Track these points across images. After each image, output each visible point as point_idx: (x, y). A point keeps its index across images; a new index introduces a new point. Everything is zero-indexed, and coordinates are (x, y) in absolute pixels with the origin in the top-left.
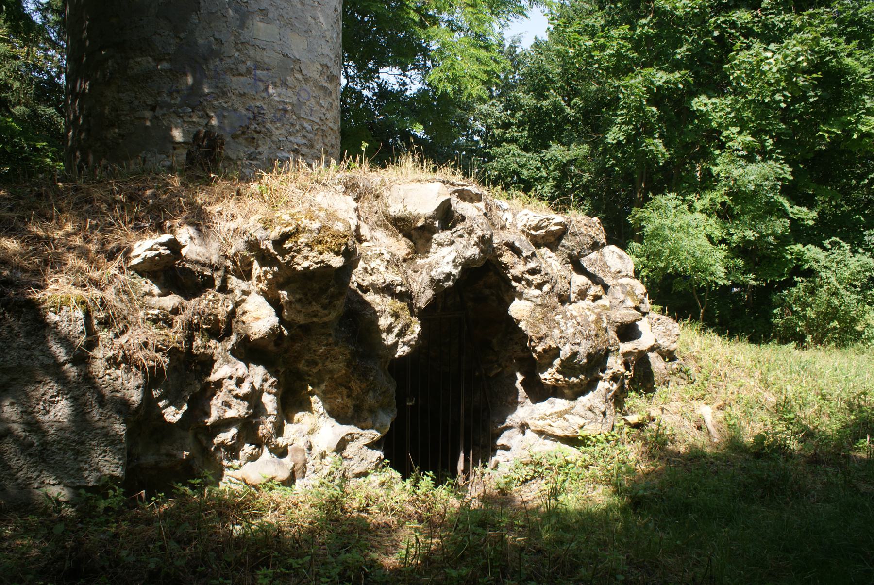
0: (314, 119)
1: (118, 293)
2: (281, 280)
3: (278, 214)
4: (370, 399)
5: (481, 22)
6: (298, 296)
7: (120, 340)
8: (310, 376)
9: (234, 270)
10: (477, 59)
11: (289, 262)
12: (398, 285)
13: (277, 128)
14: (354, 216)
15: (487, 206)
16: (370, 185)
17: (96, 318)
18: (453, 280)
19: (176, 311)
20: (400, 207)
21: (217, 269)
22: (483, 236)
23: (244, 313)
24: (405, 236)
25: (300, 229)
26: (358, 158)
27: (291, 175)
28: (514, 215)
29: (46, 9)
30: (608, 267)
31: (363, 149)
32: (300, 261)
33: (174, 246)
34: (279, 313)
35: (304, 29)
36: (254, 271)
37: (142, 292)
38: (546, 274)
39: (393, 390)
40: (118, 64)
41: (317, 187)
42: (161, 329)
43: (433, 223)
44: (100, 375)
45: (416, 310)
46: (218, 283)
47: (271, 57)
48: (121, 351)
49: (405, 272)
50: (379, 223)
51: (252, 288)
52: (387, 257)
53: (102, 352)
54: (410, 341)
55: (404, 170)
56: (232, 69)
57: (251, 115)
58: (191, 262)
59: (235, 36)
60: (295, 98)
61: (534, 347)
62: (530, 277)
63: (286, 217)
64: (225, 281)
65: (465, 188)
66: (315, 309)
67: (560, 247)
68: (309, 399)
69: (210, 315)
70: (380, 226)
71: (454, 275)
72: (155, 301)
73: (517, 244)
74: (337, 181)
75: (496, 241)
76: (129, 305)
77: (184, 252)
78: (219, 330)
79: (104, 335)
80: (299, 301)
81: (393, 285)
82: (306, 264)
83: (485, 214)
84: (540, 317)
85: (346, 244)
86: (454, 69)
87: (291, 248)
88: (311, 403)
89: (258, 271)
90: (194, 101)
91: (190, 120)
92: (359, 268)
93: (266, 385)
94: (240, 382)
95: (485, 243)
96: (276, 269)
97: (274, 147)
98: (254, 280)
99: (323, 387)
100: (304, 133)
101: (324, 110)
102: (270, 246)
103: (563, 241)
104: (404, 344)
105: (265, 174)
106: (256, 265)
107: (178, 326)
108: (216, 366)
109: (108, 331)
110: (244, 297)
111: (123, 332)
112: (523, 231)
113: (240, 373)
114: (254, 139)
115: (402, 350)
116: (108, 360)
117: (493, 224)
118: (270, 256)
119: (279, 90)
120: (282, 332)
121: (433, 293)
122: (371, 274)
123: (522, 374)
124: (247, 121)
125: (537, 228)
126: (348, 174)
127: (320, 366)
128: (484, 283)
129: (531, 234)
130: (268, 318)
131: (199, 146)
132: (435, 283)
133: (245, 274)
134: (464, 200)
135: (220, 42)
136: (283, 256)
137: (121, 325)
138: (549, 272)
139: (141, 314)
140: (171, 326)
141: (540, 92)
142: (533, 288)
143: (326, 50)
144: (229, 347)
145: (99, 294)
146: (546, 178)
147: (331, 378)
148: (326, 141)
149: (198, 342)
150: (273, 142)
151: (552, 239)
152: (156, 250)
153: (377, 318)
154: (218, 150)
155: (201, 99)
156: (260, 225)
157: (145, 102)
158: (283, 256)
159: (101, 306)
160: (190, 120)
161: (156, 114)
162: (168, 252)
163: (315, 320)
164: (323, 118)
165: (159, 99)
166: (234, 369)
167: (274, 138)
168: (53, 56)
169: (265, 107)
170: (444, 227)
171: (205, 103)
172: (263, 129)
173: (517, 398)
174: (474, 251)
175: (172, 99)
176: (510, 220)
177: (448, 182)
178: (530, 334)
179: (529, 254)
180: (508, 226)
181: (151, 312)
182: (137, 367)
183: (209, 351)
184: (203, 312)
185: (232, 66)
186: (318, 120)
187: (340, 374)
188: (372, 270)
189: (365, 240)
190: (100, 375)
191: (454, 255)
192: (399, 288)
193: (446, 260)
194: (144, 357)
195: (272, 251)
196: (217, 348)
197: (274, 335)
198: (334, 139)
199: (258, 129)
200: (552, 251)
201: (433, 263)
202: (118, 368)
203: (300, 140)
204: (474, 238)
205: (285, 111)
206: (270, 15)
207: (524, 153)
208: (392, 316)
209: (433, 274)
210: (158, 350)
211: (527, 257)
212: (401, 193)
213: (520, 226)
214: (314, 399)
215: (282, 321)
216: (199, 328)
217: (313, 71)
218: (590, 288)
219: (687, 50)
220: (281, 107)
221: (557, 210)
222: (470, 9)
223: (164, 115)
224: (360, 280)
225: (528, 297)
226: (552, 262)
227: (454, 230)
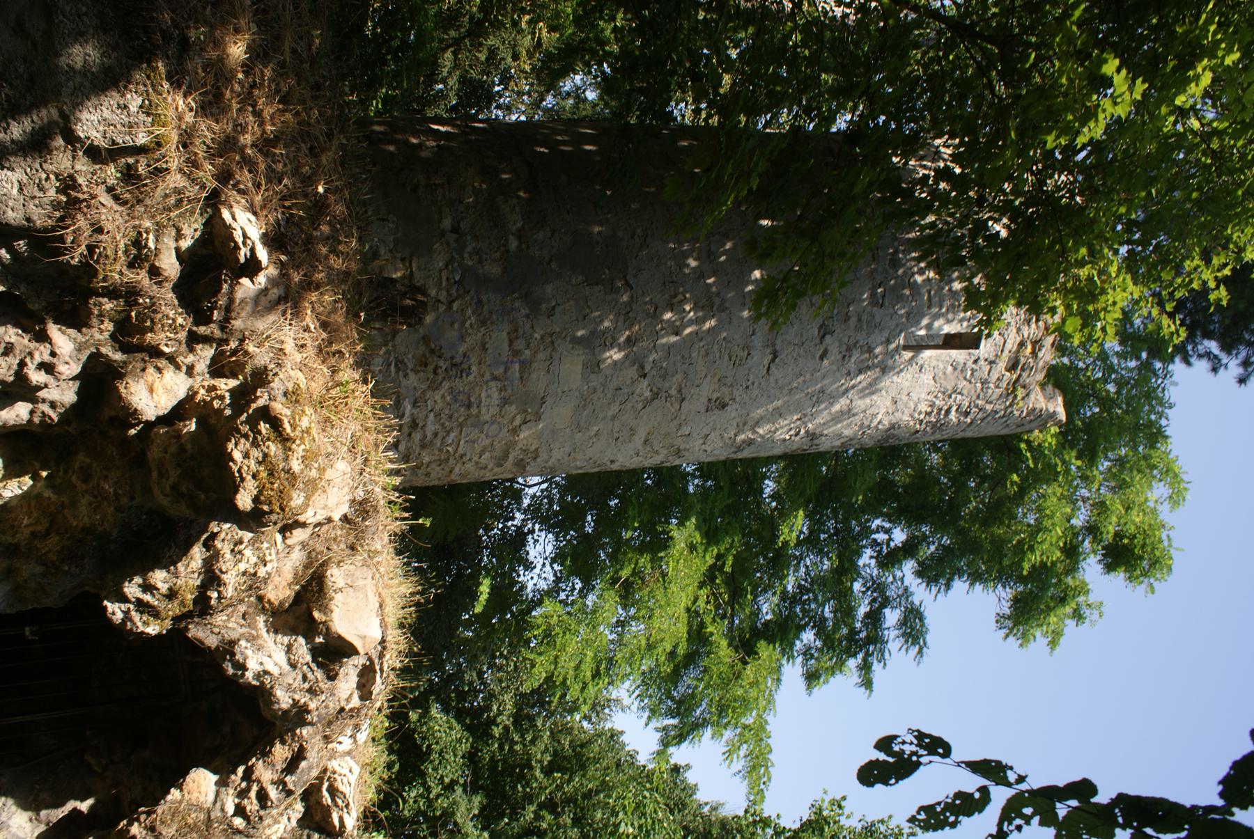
1: (177, 191)
2: (213, 421)
3: (309, 410)
4: (28, 569)
5: (630, 660)
6: (189, 446)
7: (105, 194)
8: (66, 472)
9: (223, 353)
11: (238, 431)
12: (220, 593)
13: (443, 396)
14: (320, 518)
15: (355, 713)
16: (368, 535)
17: (137, 162)
18: (235, 675)
19: (155, 272)
20: (340, 583)
21: (223, 328)
22: (309, 712)
23: (159, 370)
24: (298, 594)
25: (289, 444)
26: (407, 515)
28: (349, 753)
29: (578, 97)
31: (420, 521)
32: (241, 447)
33: (252, 267)
34: (161, 420)
35: (582, 423)
36: (223, 380)
37: (181, 225)
38: (261, 818)
39: (48, 602)
41: (358, 461)
42: (126, 252)
43: (319, 634)
44: (45, 166)
45: (183, 625)
46: (202, 330)
47: (539, 381)
48: (86, 196)
49: (241, 601)
50: (314, 554)
51: (199, 379)
52: (262, 572)
53: (84, 168)
54: (131, 620)
55: (395, 582)
56: (516, 330)
57: (458, 360)
58: (232, 292)
60: (487, 418)
61: (138, 820)
62: (253, 794)
63: (305, 423)
64: (206, 340)
65: (378, 675)
66: (171, 473)
67: (306, 832)
68: (26, 474)
69: (152, 321)
70: (309, 556)
71: (243, 675)
72: (169, 242)
73: (303, 764)
74: (370, 488)
75: (305, 731)
76: (160, 207)
77: (245, 281)
78: (131, 335)
79: (111, 173)
80: (182, 449)
81: (219, 586)
82: (237, 455)
83: (342, 709)
84: (190, 821)
85: (272, 512)
87: (260, 432)
88: (19, 476)
89: (223, 386)
92: (241, 533)
93: (45, 408)
94: (48, 368)
95: (299, 715)
96: (228, 412)
98: (210, 382)
99: (48, 493)
102: (261, 402)
104: (127, 613)
105: (370, 386)
106: (233, 383)
107: (130, 276)
108: (71, 331)
109: (117, 178)
110: (184, 369)
111: (116, 198)
112: (325, 770)
113: (62, 368)
114: (426, 366)
115: (115, 611)
116: (71, 177)
117: (330, 723)
118: (247, 404)
119: (496, 395)
120: (133, 426)
121: (213, 646)
122: (232, 551)
123: (92, 808)
124: (449, 355)
125: (333, 791)
126: (382, 502)
127: (81, 486)
128: (239, 724)
129: (322, 784)
130: (152, 405)
132: (229, 648)
133: (218, 368)
134: (361, 675)
135: (551, 313)
136: (246, 422)
137: (127, 196)
138: (266, 822)
139: (147, 224)
140: (131, 265)
142: (237, 801)
143: (557, 454)
144: (103, 350)
145: (174, 166)
147: (63, 505)
148: (433, 466)
149: (108, 305)
151: (318, 818)
152: (244, 243)
153: (165, 567)
156: (290, 386)
157: (462, 219)
158: (246, 422)
159: (156, 168)
162: (242, 260)
163: (155, 474)
164: (465, 459)
166: (67, 359)
169: (471, 378)
170: (315, 652)
172: (440, 378)
173: (47, 807)
174: (284, 699)
175: (470, 254)
176: (340, 748)
178: (160, 810)
179: (291, 786)
180: (330, 746)
181: (151, 237)
182: (62, 219)
183: (95, 321)
184: (155, 311)
185: (521, 332)
186: (461, 451)
187: (70, 518)
188: (240, 552)
189: (284, 538)
190: (45, 166)
191: (275, 671)
192: (215, 595)
193: (266, 660)
194: (79, 229)
195: (254, 406)
196: (101, 334)
197: (129, 415)
198: (437, 477)
199: (440, 371)
200: (299, 821)
201: (260, 642)
202: (58, 191)
203: (431, 428)
204: (304, 699)
205: (469, 406)
206: (593, 377)
208: (170, 589)
209: (243, 643)
210: (91, 248)
211: (285, 784)
212: (361, 583)
213: (333, 764)
214: (27, 481)
215: (149, 425)
216: (131, 306)
220: (473, 399)
221: (365, 817)
222: (643, 643)
223: (448, 245)
224: (223, 535)
225: (222, 796)
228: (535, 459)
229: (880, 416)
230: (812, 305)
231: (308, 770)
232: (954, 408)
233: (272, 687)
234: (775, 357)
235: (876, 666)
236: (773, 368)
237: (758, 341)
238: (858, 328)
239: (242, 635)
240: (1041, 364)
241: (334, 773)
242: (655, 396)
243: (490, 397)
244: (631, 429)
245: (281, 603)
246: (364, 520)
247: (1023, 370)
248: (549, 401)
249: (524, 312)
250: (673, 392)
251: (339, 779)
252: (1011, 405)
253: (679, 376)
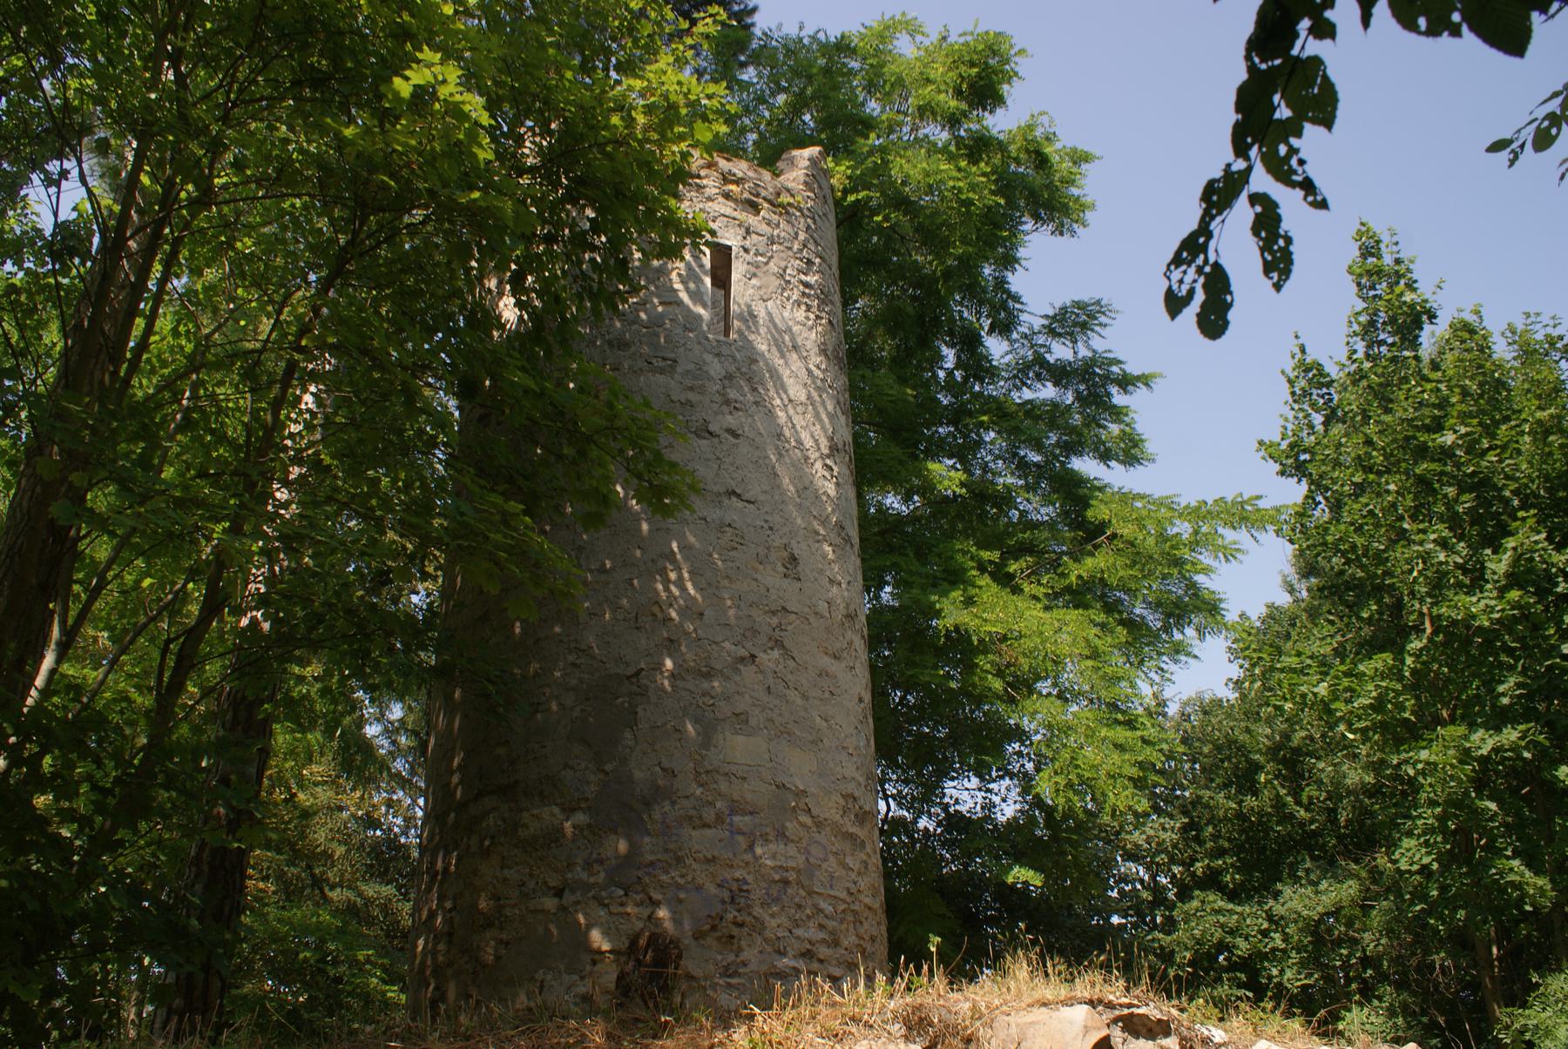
0: (837, 894)
10: (1116, 746)
13: (772, 916)
26: (925, 967)
27: (806, 1012)
31: (933, 949)
40: (504, 820)
41: (854, 1030)
55: (1012, 984)
56: (691, 818)
57: (726, 895)
60: (801, 859)
74: (889, 1015)
86: (1077, 767)
90: (629, 878)
91: (621, 909)
97: (769, 949)
105: (757, 1010)
114: (732, 937)
119: (773, 847)
126: (908, 1000)
131: (639, 963)
134: (1136, 1034)
135: (671, 773)
141: (1245, 780)
143: (850, 770)
146: (1284, 951)
148: (862, 931)
154: (671, 970)
155: (640, 873)
160: (621, 909)
161: (564, 902)
164: (854, 890)
165: (569, 875)
167: (768, 934)
168: (399, 801)
169: (750, 878)
171: (647, 879)
172: (748, 919)
175: (592, 874)
177: (1100, 1001)
185: (692, 812)
186: (843, 895)
198: (876, 927)
199: (739, 919)
205: (786, 882)
206: (753, 722)
207: (1231, 906)
212: (1014, 1030)
217: (830, 809)
219: (1519, 685)
220: (777, 877)
222: (1090, 663)
223: (578, 903)
232: (803, 277)
234: (734, 493)
236: (747, 496)
237: (714, 514)
238: (701, 390)
240: (751, 174)
242: (778, 644)
244: (820, 675)
246: (931, 1024)
247: (758, 195)
248: (781, 779)
249: (667, 807)
250: (775, 621)
252: (800, 210)
253: (755, 613)
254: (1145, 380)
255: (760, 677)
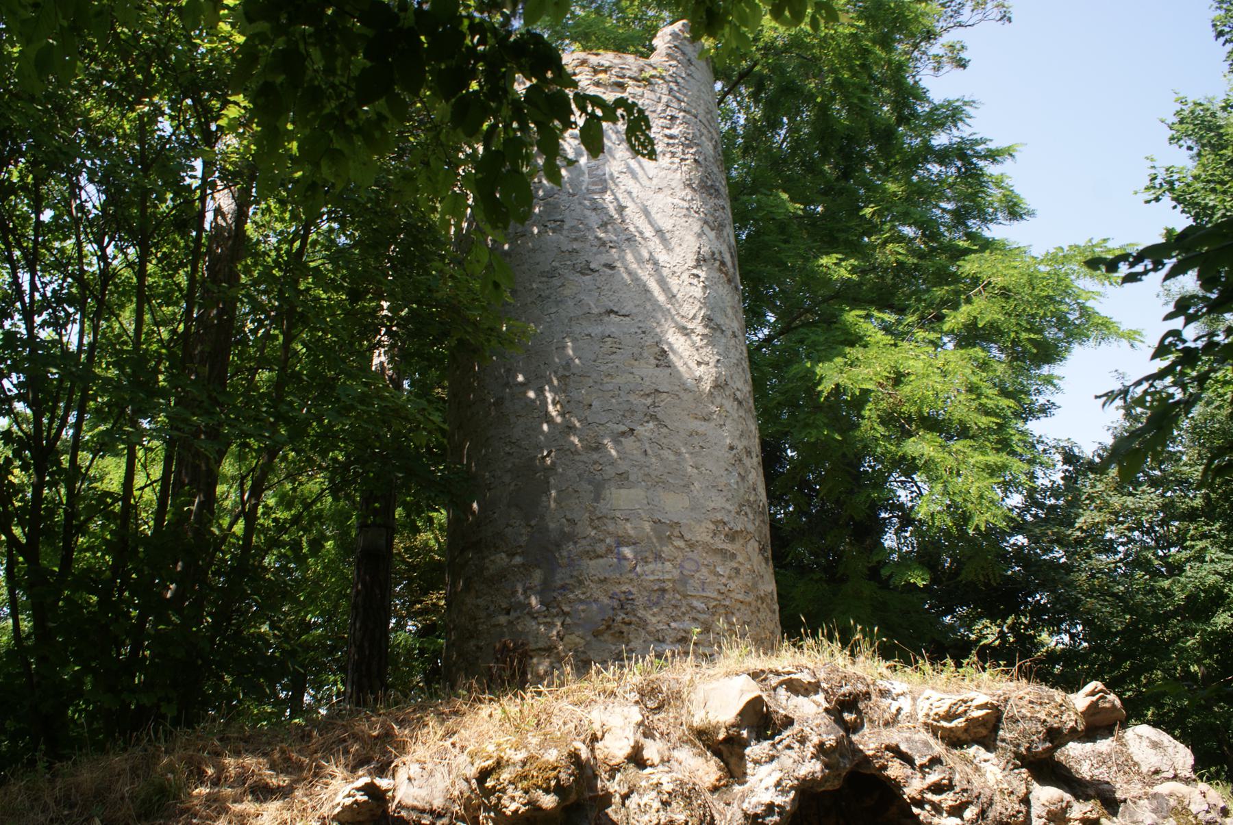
13: (654, 615)
18: (780, 814)
20: (702, 714)
22: (822, 744)
28: (914, 699)
30: (1136, 764)
35: (682, 483)
43: (739, 734)
57: (615, 603)
59: (591, 512)
62: (936, 798)
65: (793, 676)
67: (999, 743)
70: (686, 742)
73: (903, 748)
82: (513, 807)
85: (557, 777)
87: (494, 787)
100: (694, 614)
101: (724, 580)
103: (1001, 733)
125: (949, 716)
129: (942, 727)
134: (797, 693)
135: (572, 522)
142: (945, 815)
150: (649, 633)
151: (984, 732)
155: (555, 594)
158: (488, 799)
162: (366, 798)
164: (723, 589)
167: (650, 628)
169: (634, 590)
170: (760, 737)
172: (634, 619)
185: (588, 548)
186: (715, 595)
191: (777, 776)
193: (763, 785)
199: (627, 620)
204: (810, 749)
205: (664, 591)
206: (632, 478)
209: (745, 806)
211: (922, 766)
218: (1069, 805)
223: (518, 618)
226: (990, 772)
227: (777, 738)
228: (725, 523)
229: (676, 201)
230: (563, 285)
231: (922, 744)
232: (667, 132)
233: (797, 779)
234: (612, 311)
235: (992, 146)
236: (623, 312)
237: (596, 330)
238: (584, 239)
239: (739, 807)
240: (617, 61)
241: (928, 715)
242: (653, 417)
243: (654, 572)
244: (691, 435)
245: (720, 769)
247: (624, 76)
248: (657, 516)
250: (649, 401)
251: (935, 710)
252: (663, 78)
253: (632, 398)
254: (1008, 152)
255: (638, 444)
